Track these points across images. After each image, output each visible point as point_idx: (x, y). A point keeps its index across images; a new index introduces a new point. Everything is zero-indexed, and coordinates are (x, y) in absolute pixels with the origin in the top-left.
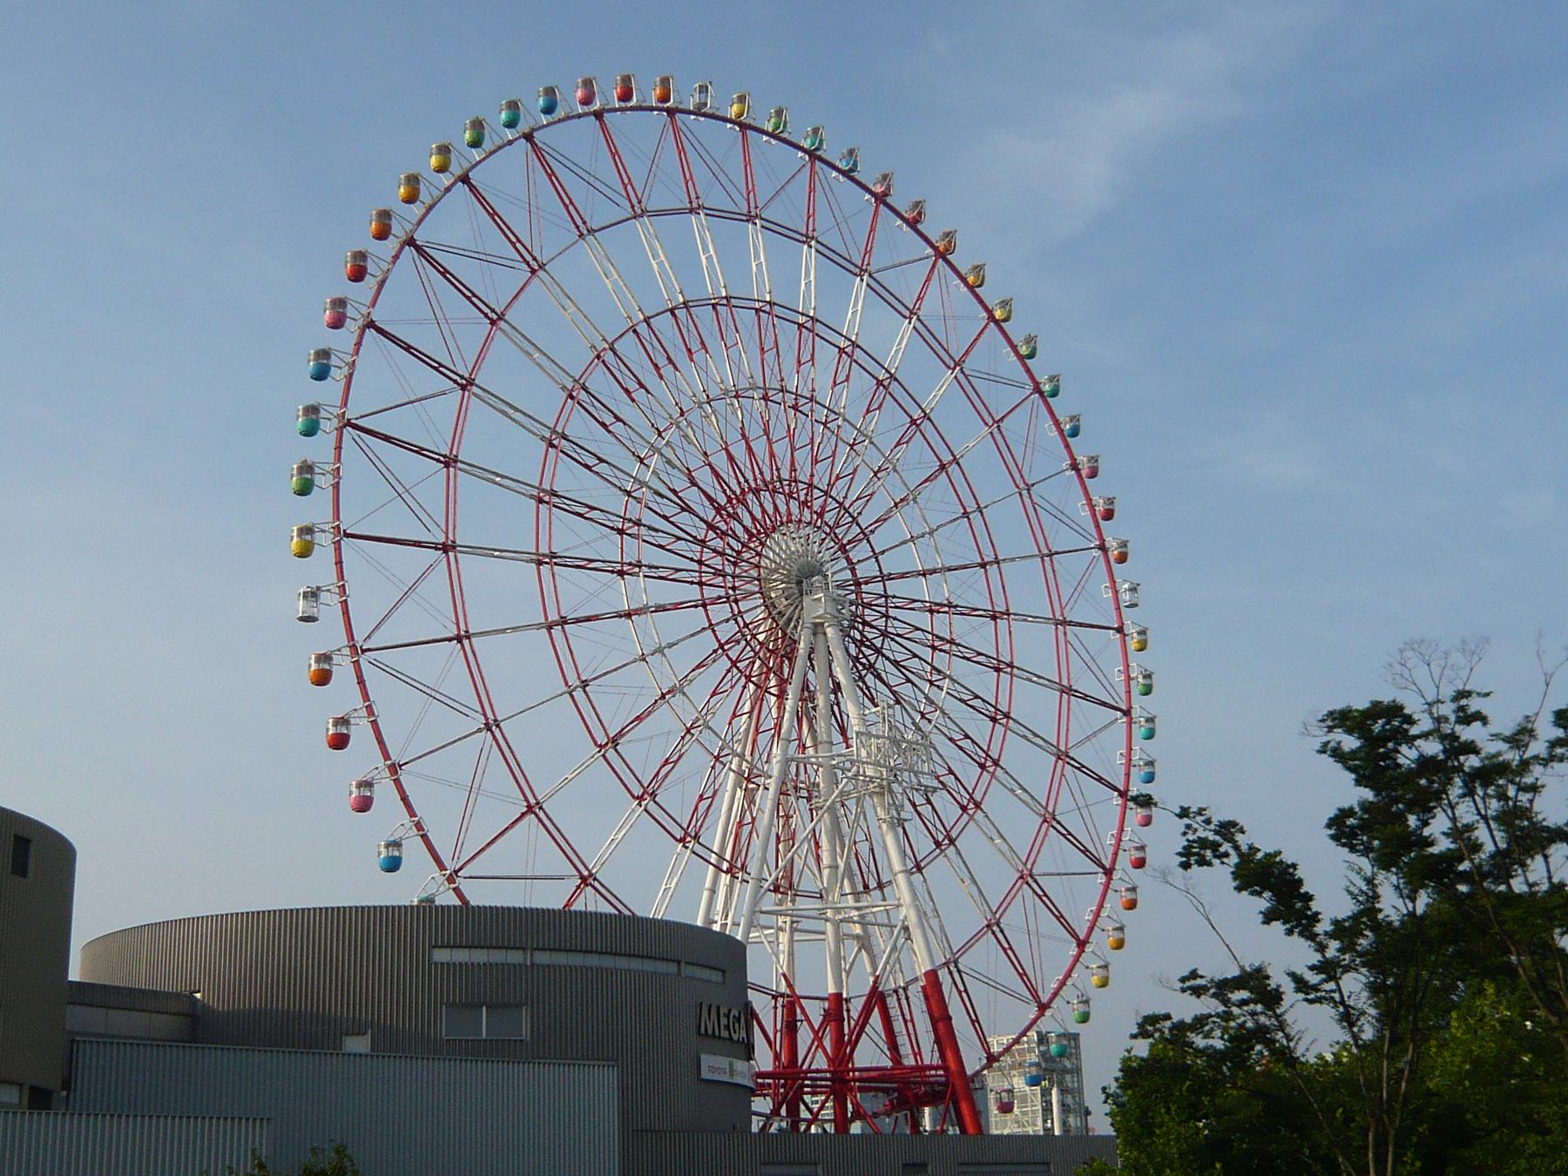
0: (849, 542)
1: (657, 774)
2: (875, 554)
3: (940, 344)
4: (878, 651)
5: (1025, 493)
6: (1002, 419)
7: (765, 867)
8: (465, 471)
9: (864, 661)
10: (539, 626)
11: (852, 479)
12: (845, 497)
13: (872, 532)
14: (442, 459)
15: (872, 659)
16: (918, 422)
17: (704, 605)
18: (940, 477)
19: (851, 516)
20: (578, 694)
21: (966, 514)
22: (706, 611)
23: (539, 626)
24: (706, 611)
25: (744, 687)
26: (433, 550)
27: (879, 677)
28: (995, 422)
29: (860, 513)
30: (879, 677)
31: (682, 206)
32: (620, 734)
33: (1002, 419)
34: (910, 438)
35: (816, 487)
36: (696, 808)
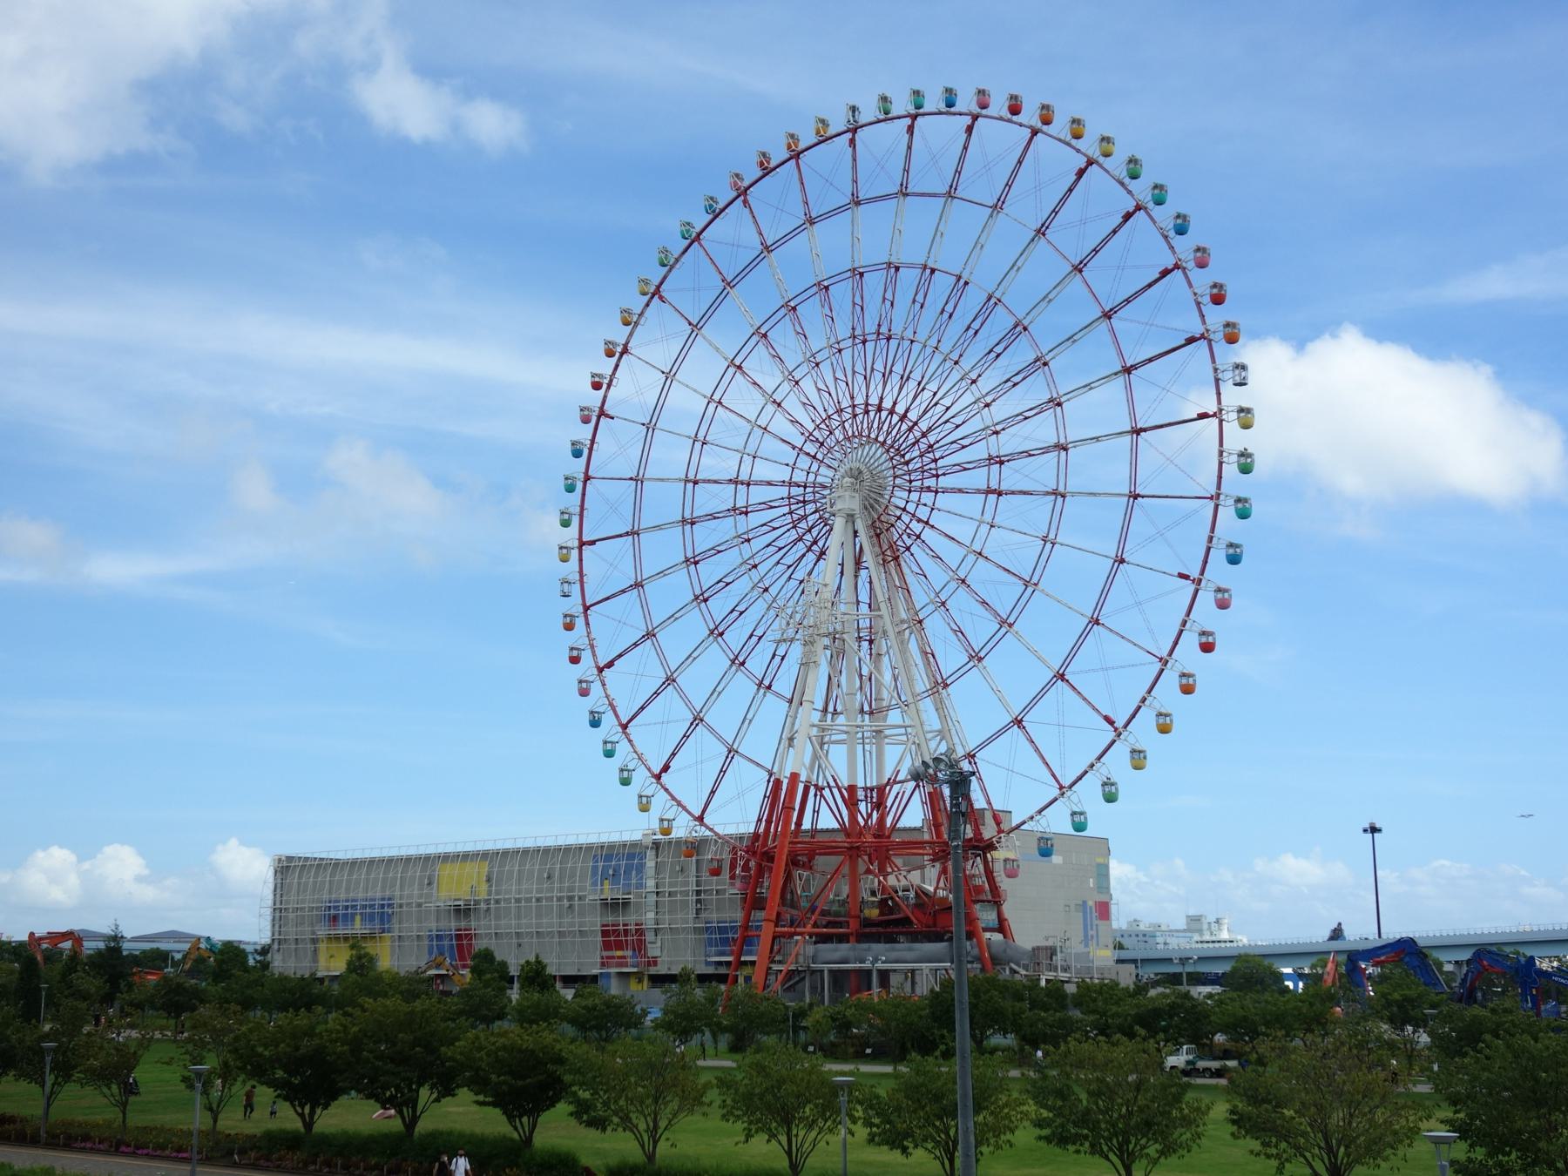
2: (793, 468)
7: (949, 1172)
18: (701, 478)
20: (698, 445)
28: (637, 481)
31: (704, 728)
32: (1047, 493)
33: (631, 479)
34: (760, 504)
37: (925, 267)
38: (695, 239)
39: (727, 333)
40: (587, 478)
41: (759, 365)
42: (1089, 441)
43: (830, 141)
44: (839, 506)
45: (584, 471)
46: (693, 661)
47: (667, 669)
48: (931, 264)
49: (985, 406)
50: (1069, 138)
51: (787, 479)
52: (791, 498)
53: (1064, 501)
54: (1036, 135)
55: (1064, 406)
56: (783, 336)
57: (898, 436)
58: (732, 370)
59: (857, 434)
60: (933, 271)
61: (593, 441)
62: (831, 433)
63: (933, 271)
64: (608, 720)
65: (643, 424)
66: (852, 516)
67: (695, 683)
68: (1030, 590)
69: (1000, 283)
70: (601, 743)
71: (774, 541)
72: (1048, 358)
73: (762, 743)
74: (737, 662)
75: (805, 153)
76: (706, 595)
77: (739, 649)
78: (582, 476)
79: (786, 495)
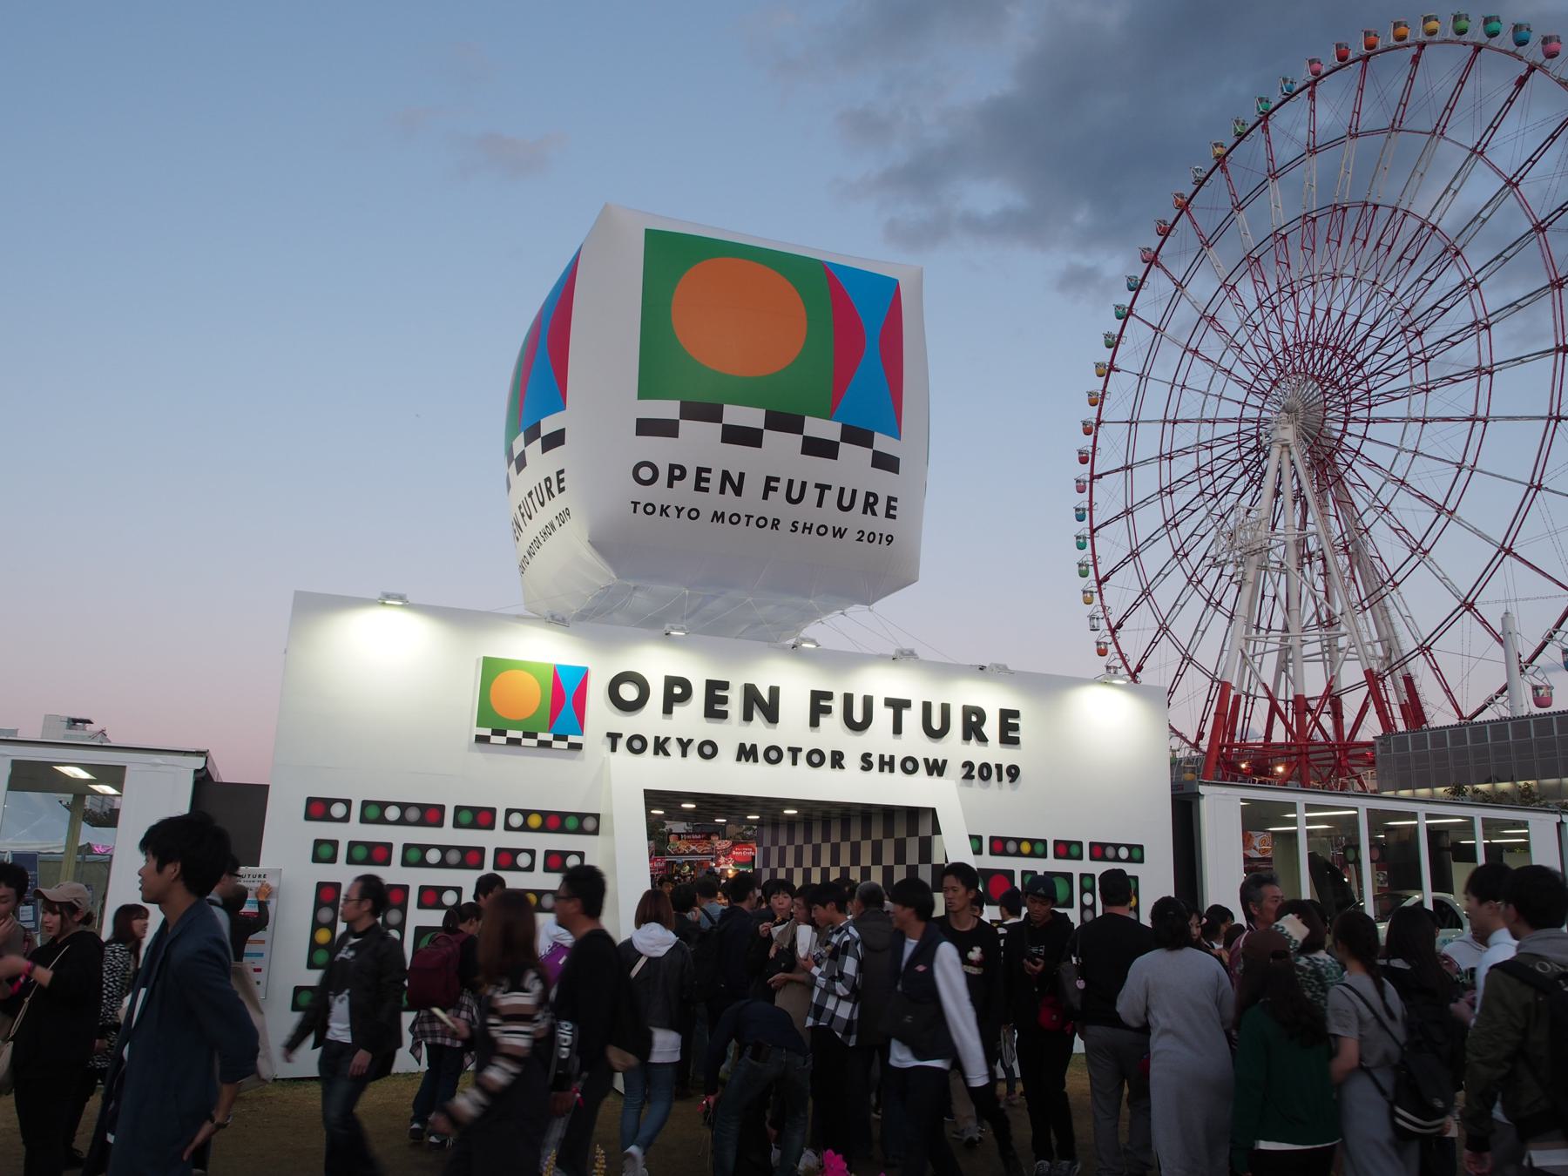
0: (1254, 422)
1: (1466, 379)
3: (1554, 268)
4: (1275, 358)
5: (1146, 374)
6: (1127, 422)
8: (1516, 195)
9: (1287, 357)
10: (1459, 521)
11: (1223, 455)
12: (1234, 449)
13: (1235, 419)
14: (1428, 654)
15: (1281, 355)
16: (1168, 456)
17: (1358, 452)
19: (1239, 436)
20: (1177, 390)
21: (1183, 387)
22: (1359, 449)
23: (1459, 521)
24: (1359, 449)
25: (1376, 388)
26: (1479, 611)
27: (1284, 341)
29: (1234, 434)
30: (1284, 341)
32: (1468, 419)
33: (1127, 422)
35: (1367, 383)
36: (1462, 340)
37: (1366, 204)
38: (1184, 207)
39: (1224, 256)
40: (1099, 423)
41: (1247, 290)
42: (1512, 363)
43: (1295, 98)
44: (1274, 436)
45: (1089, 472)
46: (1202, 635)
47: (1158, 615)
48: (1372, 200)
49: (1416, 335)
50: (1512, 47)
51: (1238, 416)
52: (1241, 433)
53: (1485, 426)
54: (1480, 51)
55: (1492, 328)
56: (1246, 289)
57: (1342, 336)
58: (1204, 323)
59: (1303, 371)
60: (1376, 207)
61: (1094, 447)
62: (1257, 377)
63: (1376, 207)
64: (1103, 625)
65: (1138, 375)
66: (1288, 446)
67: (1165, 595)
68: (1443, 519)
69: (1434, 209)
70: (1095, 644)
71: (1187, 505)
72: (1479, 278)
73: (1207, 654)
74: (1212, 601)
75: (1275, 113)
76: (1178, 519)
77: (1213, 587)
78: (1094, 421)
79: (1236, 430)
